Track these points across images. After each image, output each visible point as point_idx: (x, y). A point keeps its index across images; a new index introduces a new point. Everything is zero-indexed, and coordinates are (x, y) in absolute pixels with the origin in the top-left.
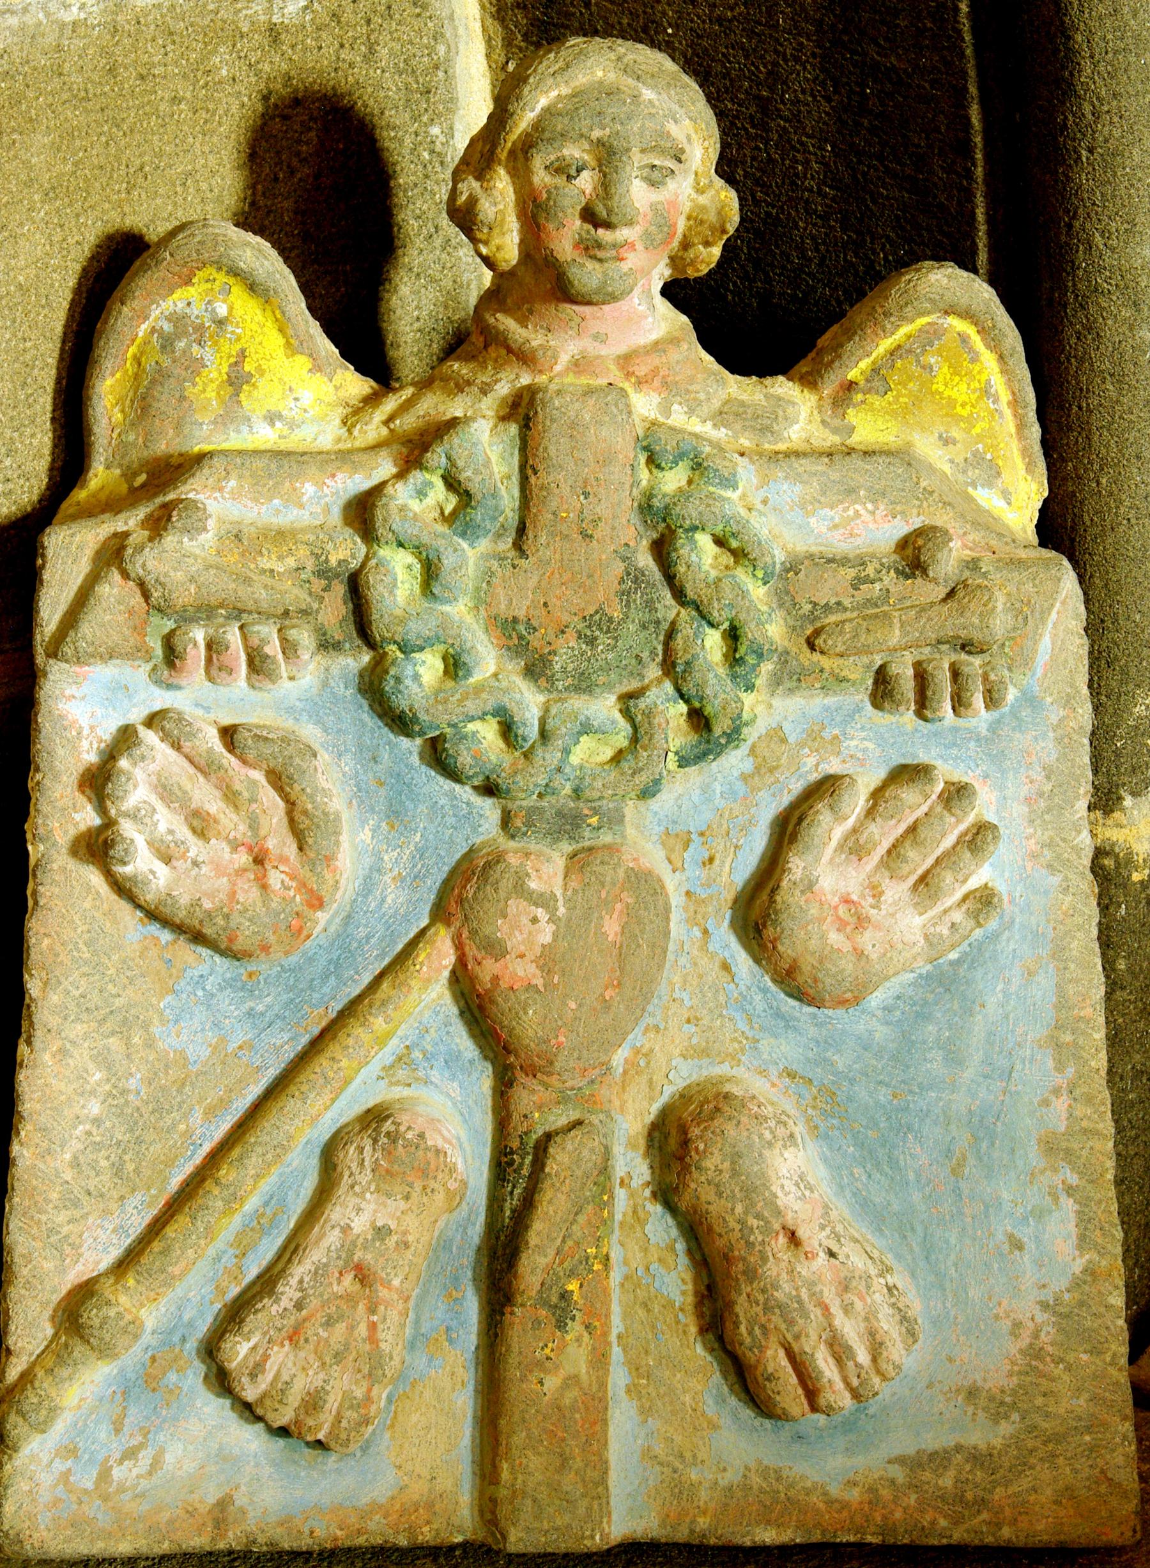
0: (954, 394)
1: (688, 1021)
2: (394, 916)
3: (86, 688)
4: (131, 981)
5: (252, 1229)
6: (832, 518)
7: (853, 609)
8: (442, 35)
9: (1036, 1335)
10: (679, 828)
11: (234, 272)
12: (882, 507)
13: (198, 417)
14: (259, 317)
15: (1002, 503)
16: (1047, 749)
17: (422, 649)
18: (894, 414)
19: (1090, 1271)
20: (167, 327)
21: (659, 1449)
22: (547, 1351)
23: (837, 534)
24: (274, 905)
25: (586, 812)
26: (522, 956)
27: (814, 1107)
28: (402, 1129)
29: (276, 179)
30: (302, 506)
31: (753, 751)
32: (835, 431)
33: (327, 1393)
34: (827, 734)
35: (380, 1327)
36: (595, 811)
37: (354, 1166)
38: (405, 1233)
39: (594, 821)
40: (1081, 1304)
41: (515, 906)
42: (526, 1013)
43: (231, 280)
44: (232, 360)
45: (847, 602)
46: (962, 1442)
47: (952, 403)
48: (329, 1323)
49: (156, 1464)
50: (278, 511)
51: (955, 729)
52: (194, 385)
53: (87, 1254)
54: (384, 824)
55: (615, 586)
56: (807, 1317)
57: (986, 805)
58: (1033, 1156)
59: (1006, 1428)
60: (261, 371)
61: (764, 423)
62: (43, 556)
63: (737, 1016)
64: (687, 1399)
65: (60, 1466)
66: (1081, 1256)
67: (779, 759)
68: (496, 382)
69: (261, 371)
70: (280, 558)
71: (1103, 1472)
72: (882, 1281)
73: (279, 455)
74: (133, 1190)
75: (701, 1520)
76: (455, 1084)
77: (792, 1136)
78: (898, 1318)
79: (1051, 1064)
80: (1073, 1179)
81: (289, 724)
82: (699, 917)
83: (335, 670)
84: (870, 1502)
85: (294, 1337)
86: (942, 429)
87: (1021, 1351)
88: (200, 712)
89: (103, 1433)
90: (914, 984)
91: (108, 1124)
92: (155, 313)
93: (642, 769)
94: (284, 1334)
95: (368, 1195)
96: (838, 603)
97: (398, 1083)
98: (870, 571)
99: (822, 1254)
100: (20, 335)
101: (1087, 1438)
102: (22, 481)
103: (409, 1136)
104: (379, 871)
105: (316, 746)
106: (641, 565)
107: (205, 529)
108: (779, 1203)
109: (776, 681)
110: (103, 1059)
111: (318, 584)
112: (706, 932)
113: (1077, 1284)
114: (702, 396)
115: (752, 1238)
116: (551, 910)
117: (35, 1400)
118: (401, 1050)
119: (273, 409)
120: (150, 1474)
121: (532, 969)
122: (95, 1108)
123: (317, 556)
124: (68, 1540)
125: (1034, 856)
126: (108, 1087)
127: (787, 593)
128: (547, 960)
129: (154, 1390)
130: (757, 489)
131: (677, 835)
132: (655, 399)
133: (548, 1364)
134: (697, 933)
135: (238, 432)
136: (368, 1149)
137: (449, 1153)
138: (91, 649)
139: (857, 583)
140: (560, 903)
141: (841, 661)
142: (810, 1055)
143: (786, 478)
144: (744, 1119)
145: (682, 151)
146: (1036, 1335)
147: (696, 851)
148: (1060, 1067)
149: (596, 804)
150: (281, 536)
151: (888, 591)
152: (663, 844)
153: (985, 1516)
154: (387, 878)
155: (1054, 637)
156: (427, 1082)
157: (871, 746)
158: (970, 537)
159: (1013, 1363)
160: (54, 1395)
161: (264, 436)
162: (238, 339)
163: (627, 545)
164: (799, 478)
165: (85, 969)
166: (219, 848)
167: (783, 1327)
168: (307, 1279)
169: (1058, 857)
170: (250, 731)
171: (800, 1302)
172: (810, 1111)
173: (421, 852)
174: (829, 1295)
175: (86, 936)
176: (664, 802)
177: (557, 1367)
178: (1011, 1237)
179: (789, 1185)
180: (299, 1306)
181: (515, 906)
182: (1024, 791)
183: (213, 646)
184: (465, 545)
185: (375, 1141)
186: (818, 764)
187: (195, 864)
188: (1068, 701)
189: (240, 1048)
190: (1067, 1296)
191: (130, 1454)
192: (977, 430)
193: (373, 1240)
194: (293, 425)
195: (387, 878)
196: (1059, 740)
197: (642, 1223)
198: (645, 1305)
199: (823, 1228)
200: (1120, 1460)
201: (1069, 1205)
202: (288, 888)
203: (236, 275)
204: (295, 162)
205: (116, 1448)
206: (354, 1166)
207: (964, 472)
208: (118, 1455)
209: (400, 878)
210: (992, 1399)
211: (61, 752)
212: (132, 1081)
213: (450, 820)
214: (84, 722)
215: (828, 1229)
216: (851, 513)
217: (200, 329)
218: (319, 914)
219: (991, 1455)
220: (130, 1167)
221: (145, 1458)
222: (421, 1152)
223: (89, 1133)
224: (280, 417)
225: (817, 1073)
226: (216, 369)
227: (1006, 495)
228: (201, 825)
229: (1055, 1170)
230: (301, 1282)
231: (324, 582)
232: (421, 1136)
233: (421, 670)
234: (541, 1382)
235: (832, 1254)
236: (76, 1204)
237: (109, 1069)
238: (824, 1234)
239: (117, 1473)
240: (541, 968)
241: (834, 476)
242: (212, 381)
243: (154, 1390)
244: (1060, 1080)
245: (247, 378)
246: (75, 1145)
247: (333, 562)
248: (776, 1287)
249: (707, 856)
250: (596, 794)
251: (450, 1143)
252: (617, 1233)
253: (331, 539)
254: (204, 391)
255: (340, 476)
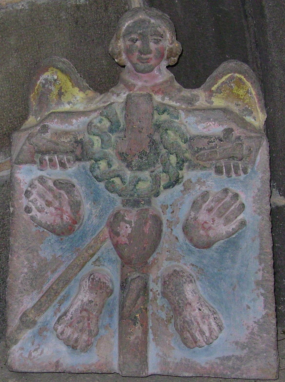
0: (239, 93)
1: (167, 252)
2: (95, 225)
3: (22, 171)
4: (34, 240)
5: (62, 299)
6: (204, 126)
7: (208, 149)
8: (127, 3)
9: (253, 329)
10: (165, 204)
11: (57, 68)
12: (216, 123)
13: (51, 103)
14: (65, 78)
15: (253, 120)
16: (258, 184)
17: (99, 161)
18: (223, 98)
19: (267, 314)
20: (44, 82)
21: (161, 353)
22: (131, 330)
23: (205, 130)
24: (64, 223)
25: (141, 200)
26: (124, 236)
27: (198, 273)
28: (95, 277)
29: (81, 42)
30: (72, 125)
31: (184, 184)
32: (209, 103)
33: (78, 339)
34: (202, 181)
35: (91, 324)
36: (143, 200)
37: (84, 286)
38: (96, 302)
39: (143, 202)
40: (264, 322)
41: (122, 224)
42: (125, 250)
43: (57, 70)
44: (59, 89)
45: (206, 148)
46: (234, 354)
47: (238, 95)
48: (78, 323)
49: (42, 352)
50: (67, 127)
51: (235, 179)
52: (50, 95)
53: (24, 304)
54: (92, 203)
55: (147, 144)
56: (193, 324)
57: (243, 197)
58: (253, 286)
59: (245, 351)
60: (66, 92)
61: (190, 101)
62: (12, 139)
63: (179, 250)
64: (167, 342)
65: (20, 352)
66: (265, 310)
67: (190, 187)
68: (120, 93)
69: (66, 92)
70: (66, 139)
71: (268, 362)
72: (213, 316)
73: (68, 113)
74: (35, 290)
75: (170, 370)
76: (111, 266)
77: (191, 281)
78: (216, 325)
79: (258, 263)
80: (263, 292)
81: (69, 178)
82: (170, 226)
83: (81, 166)
84: (211, 368)
85: (70, 325)
86: (236, 102)
87: (249, 333)
88: (48, 176)
89: (30, 344)
90: (224, 243)
91: (29, 274)
92: (41, 78)
93: (153, 190)
94: (68, 325)
95: (87, 293)
96: (204, 148)
97: (96, 266)
98: (212, 139)
99: (197, 310)
100: (11, 85)
101: (265, 354)
102: (14, 119)
103: (96, 279)
104: (91, 214)
105: (75, 184)
106: (154, 139)
107: (47, 132)
108: (187, 297)
109: (188, 168)
110: (28, 259)
111: (75, 145)
112: (172, 230)
113: (263, 317)
114: (174, 95)
115: (180, 305)
116: (131, 225)
117: (12, 337)
118: (97, 258)
119: (69, 101)
120: (41, 354)
121: (126, 239)
122: (26, 270)
123: (75, 138)
124: (23, 368)
125: (255, 211)
126: (28, 265)
127: (191, 145)
128: (130, 237)
129: (41, 336)
130: (185, 119)
131: (165, 206)
132: (160, 96)
133: (132, 333)
134: (170, 230)
135: (61, 107)
136: (87, 282)
137: (107, 283)
138: (22, 162)
139: (209, 142)
140: (133, 223)
141: (204, 162)
142: (198, 260)
143: (192, 116)
144: (178, 277)
145: (162, 35)
146: (253, 329)
147: (169, 210)
148: (260, 264)
149: (143, 198)
150: (66, 133)
151: (216, 145)
152: (161, 208)
153: (239, 372)
154: (93, 216)
155: (260, 157)
156: (103, 265)
157: (213, 183)
158: (239, 130)
159: (247, 336)
160: (17, 336)
161: (67, 107)
162: (60, 84)
163: (151, 134)
164: (195, 116)
165: (23, 238)
166: (52, 209)
167: (187, 326)
168: (73, 312)
169: (261, 212)
170: (58, 181)
171: (191, 320)
172: (197, 274)
173: (102, 210)
174: (199, 319)
175: (23, 230)
176: (161, 197)
177: (133, 334)
178: (247, 305)
179: (190, 293)
180: (71, 318)
181: (122, 224)
182: (253, 195)
183: (51, 160)
184: (111, 135)
185: (89, 280)
186: (199, 189)
187: (46, 213)
188: (264, 172)
189: (59, 256)
190: (261, 320)
191: (36, 350)
192: (246, 102)
193: (89, 303)
194: (74, 104)
195: (93, 216)
196: (262, 182)
197: (156, 300)
198: (157, 320)
199: (198, 303)
200: (273, 360)
201: (262, 298)
202: (67, 219)
203: (58, 69)
204: (86, 37)
205: (33, 348)
206: (84, 286)
207: (243, 112)
208: (33, 350)
209: (96, 216)
210: (242, 344)
211: (16, 186)
212: (34, 264)
213: (109, 202)
214: (21, 178)
215: (199, 304)
216: (209, 124)
217: (50, 82)
218: (76, 225)
219: (241, 358)
220: (34, 284)
221: (39, 351)
222: (99, 283)
223: (24, 276)
224: (71, 103)
225: (199, 265)
226: (55, 91)
227: (254, 118)
228: (49, 204)
229: (259, 289)
230: (72, 313)
231: (77, 144)
232: (100, 279)
233: (100, 166)
234: (130, 338)
235: (200, 310)
236: (22, 293)
237: (29, 261)
238: (198, 305)
239: (33, 354)
240: (128, 239)
241: (205, 115)
242: (54, 94)
243: (41, 336)
244: (261, 267)
245: (63, 94)
246: (21, 279)
247: (79, 139)
248: (186, 317)
249: (172, 211)
250: (143, 196)
251: (107, 280)
252: (150, 302)
253: (79, 133)
254: (52, 97)
255: (82, 118)
